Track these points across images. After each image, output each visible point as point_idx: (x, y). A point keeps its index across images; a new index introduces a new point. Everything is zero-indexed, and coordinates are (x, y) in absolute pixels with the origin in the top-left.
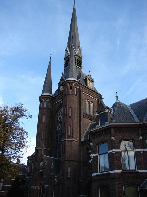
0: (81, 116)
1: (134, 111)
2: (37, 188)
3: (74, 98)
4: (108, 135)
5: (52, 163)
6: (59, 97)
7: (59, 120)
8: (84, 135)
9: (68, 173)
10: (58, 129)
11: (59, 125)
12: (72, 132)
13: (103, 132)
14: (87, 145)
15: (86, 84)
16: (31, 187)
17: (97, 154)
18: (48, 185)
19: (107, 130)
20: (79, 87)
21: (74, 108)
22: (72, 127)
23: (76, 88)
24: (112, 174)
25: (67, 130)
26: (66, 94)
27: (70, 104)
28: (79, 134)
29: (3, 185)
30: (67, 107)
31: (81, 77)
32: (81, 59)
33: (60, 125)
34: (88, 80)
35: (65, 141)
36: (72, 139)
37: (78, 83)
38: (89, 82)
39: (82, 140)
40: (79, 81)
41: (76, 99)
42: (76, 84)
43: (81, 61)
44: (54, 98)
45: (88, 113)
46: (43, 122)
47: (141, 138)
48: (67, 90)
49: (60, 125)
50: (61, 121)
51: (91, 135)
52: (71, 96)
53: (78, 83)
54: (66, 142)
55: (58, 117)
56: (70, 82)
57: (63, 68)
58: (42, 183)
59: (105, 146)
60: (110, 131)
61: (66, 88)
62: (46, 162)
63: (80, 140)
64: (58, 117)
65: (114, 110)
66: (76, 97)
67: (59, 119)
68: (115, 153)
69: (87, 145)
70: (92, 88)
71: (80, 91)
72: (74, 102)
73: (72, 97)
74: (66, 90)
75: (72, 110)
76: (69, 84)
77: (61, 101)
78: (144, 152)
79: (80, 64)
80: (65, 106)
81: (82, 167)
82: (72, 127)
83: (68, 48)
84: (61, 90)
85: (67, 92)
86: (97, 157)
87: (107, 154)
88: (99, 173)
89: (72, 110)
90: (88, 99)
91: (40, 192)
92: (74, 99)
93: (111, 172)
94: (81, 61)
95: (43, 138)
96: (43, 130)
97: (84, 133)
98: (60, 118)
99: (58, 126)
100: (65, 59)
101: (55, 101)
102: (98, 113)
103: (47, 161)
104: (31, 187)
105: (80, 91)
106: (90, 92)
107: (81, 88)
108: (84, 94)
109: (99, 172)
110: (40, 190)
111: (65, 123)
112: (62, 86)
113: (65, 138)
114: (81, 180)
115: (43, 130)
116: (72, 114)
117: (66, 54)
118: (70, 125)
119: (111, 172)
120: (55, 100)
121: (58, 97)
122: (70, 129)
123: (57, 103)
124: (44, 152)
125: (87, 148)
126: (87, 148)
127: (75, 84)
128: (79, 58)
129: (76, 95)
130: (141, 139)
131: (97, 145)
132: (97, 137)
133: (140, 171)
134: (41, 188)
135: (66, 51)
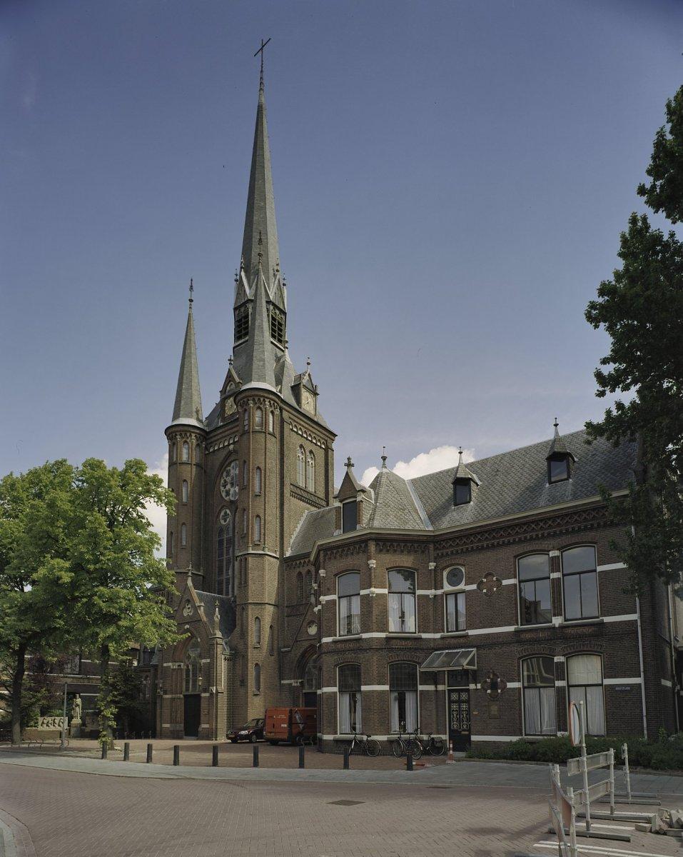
0: (285, 491)
1: (421, 497)
2: (180, 666)
3: (268, 441)
4: (361, 555)
5: (217, 609)
6: (223, 432)
7: (227, 498)
8: (292, 541)
9: (369, 736)
10: (222, 522)
11: (226, 513)
12: (264, 535)
13: (352, 548)
14: (299, 567)
15: (298, 401)
16: (165, 665)
17: (334, 597)
18: (282, 725)
19: (361, 544)
20: (281, 409)
21: (267, 470)
22: (263, 521)
23: (272, 412)
24: (365, 639)
25: (250, 526)
26: (246, 428)
27: (256, 460)
28: (278, 539)
29: (80, 662)
30: (249, 465)
31: (285, 380)
32: (283, 317)
33: (228, 512)
34: (303, 390)
35: (246, 556)
36: (263, 550)
37: (277, 400)
38: (305, 395)
39: (288, 554)
40: (280, 392)
41: (273, 445)
42: (272, 402)
43: (283, 323)
44: (208, 433)
45: (302, 484)
46: (182, 502)
47: (432, 565)
48: (249, 417)
49: (228, 512)
50: (232, 502)
51: (322, 552)
52: (261, 437)
53: (277, 400)
54: (250, 559)
55: (222, 488)
56: (257, 396)
57: (230, 341)
58: (192, 655)
59: (354, 579)
60: (366, 546)
61: (246, 410)
62: (200, 606)
63: (282, 552)
64: (222, 488)
65: (377, 494)
66: (274, 439)
67: (224, 494)
68: (374, 595)
69: (299, 567)
70: (313, 412)
71: (282, 421)
72: (268, 453)
73: (263, 440)
74: (246, 418)
75: (263, 475)
76: (254, 400)
77: (229, 445)
78: (435, 596)
79: (279, 329)
80: (245, 462)
81: (286, 619)
82: (263, 521)
83: (243, 274)
84: (229, 412)
85: (249, 422)
86: (334, 601)
87: (359, 598)
88: (338, 638)
89: (263, 475)
90: (301, 446)
91: (188, 675)
92: (268, 446)
93: (365, 636)
94: (283, 323)
95: (184, 543)
96: (184, 524)
97: (291, 534)
98: (228, 493)
99: (222, 514)
100: (235, 309)
101: (212, 443)
102: (341, 501)
103: (203, 604)
104: (165, 665)
105: (282, 421)
106: (307, 426)
107: (284, 412)
108: (292, 430)
109: (338, 635)
110: (188, 670)
111: (244, 510)
112: (230, 401)
113: (247, 549)
114: (284, 647)
115: (184, 524)
116: (263, 485)
117: (238, 294)
118: (258, 516)
119: (365, 636)
120: (215, 439)
121: (221, 431)
122: (256, 527)
123: (219, 449)
124: (193, 581)
125: (300, 573)
126: (300, 573)
127: (269, 402)
128: (278, 312)
129: (273, 435)
130: (433, 568)
131: (336, 575)
132: (335, 558)
133: (424, 636)
134: (190, 667)
135: (236, 280)
